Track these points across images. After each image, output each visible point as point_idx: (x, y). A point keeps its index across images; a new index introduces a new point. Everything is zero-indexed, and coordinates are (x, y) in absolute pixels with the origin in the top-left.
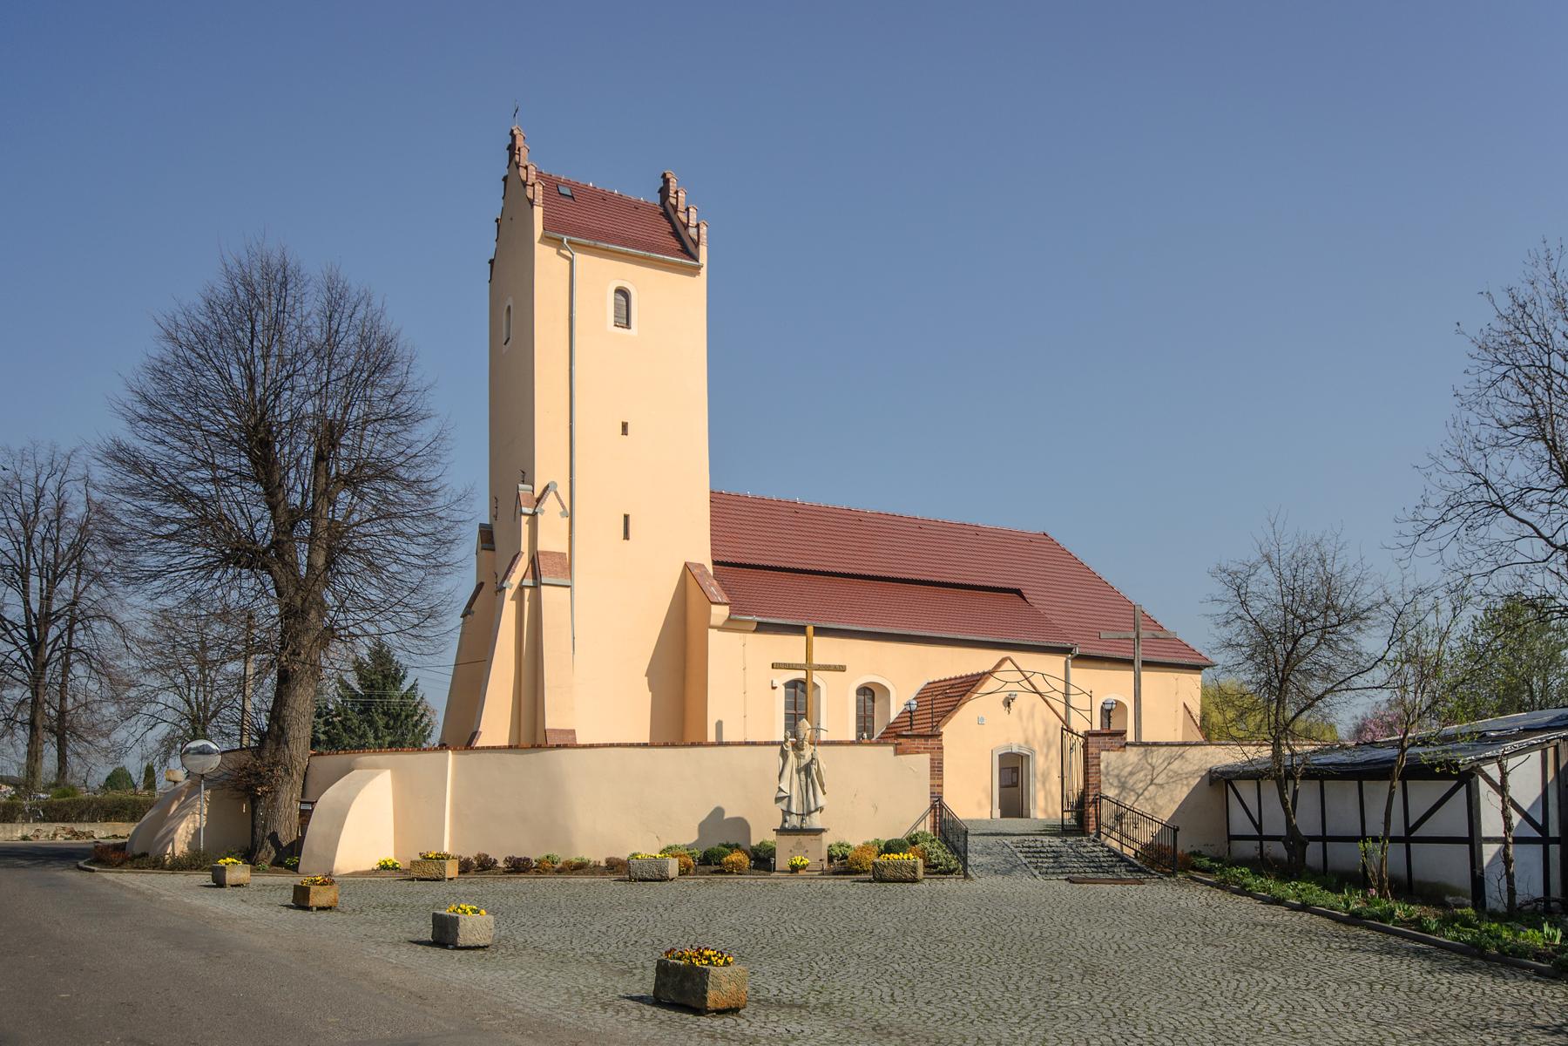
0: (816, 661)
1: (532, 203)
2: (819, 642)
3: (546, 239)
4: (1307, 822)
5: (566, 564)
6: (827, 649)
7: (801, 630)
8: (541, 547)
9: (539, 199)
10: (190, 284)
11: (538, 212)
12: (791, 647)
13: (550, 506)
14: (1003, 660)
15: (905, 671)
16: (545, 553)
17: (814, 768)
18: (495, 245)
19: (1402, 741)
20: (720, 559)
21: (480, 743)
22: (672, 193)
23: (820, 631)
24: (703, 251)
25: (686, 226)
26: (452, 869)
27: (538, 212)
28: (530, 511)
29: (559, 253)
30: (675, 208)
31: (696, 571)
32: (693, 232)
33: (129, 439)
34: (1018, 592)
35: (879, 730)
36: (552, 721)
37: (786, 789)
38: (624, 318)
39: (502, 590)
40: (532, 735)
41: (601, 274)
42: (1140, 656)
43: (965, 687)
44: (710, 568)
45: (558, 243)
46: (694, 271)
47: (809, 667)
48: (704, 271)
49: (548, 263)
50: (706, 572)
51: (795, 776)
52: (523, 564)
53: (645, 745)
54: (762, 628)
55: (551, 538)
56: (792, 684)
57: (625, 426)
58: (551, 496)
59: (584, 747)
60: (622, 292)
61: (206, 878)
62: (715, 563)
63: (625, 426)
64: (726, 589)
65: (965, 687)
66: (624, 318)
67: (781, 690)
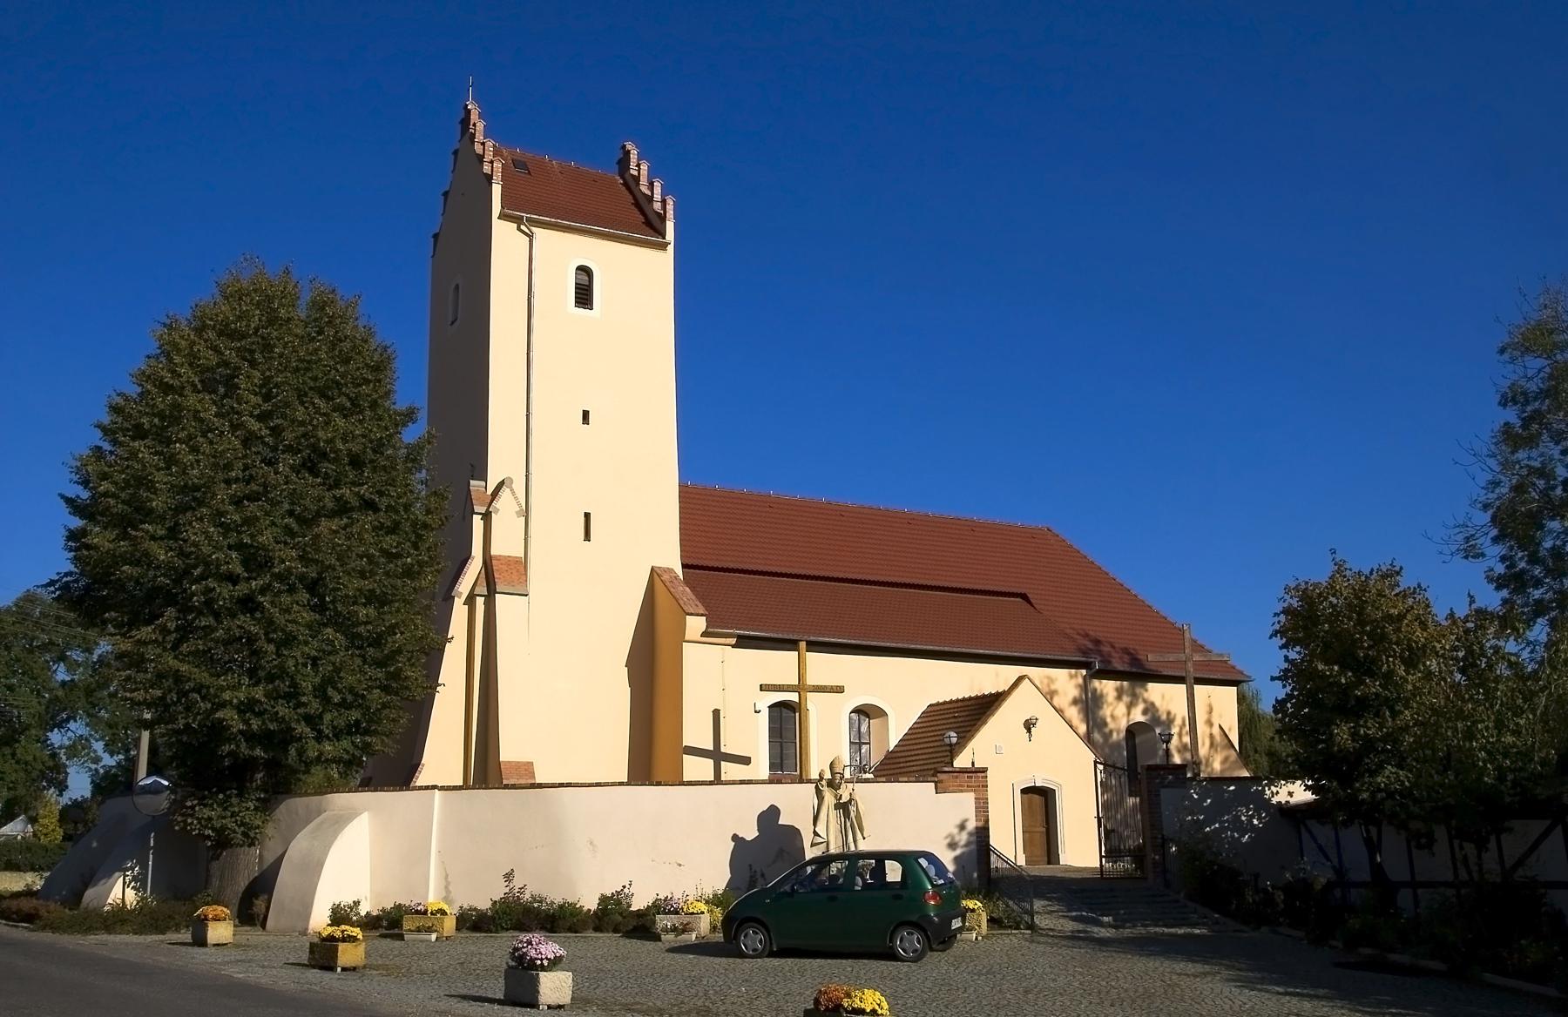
0: (811, 680)
1: (489, 178)
2: (815, 659)
3: (502, 217)
4: (1397, 870)
5: (520, 566)
6: (823, 667)
7: (790, 645)
8: (495, 551)
9: (497, 176)
10: (190, 292)
11: (497, 190)
12: (780, 665)
13: (506, 507)
14: (1020, 679)
15: (908, 688)
16: (499, 558)
17: (852, 809)
18: (440, 219)
19: (162, 698)
20: (690, 562)
21: (422, 779)
22: (633, 165)
23: (814, 646)
24: (670, 227)
25: (650, 199)
26: (449, 924)
27: (497, 190)
28: (483, 510)
29: (519, 229)
30: (637, 179)
31: (666, 577)
32: (657, 206)
33: (100, 443)
34: (1024, 597)
35: (876, 758)
36: (510, 750)
37: (823, 834)
38: (584, 296)
39: (449, 600)
40: (485, 767)
41: (561, 251)
42: (1192, 672)
43: (981, 708)
44: (679, 571)
45: (518, 221)
46: (663, 246)
47: (800, 688)
48: (671, 248)
49: (505, 238)
50: (676, 577)
51: (833, 813)
52: (474, 568)
53: (621, 784)
54: (743, 642)
55: (506, 543)
56: (776, 708)
57: (586, 415)
58: (505, 493)
59: (733, 783)
60: (584, 271)
61: (186, 936)
62: (684, 566)
63: (586, 415)
64: (701, 597)
65: (981, 708)
66: (584, 296)
67: (764, 719)
